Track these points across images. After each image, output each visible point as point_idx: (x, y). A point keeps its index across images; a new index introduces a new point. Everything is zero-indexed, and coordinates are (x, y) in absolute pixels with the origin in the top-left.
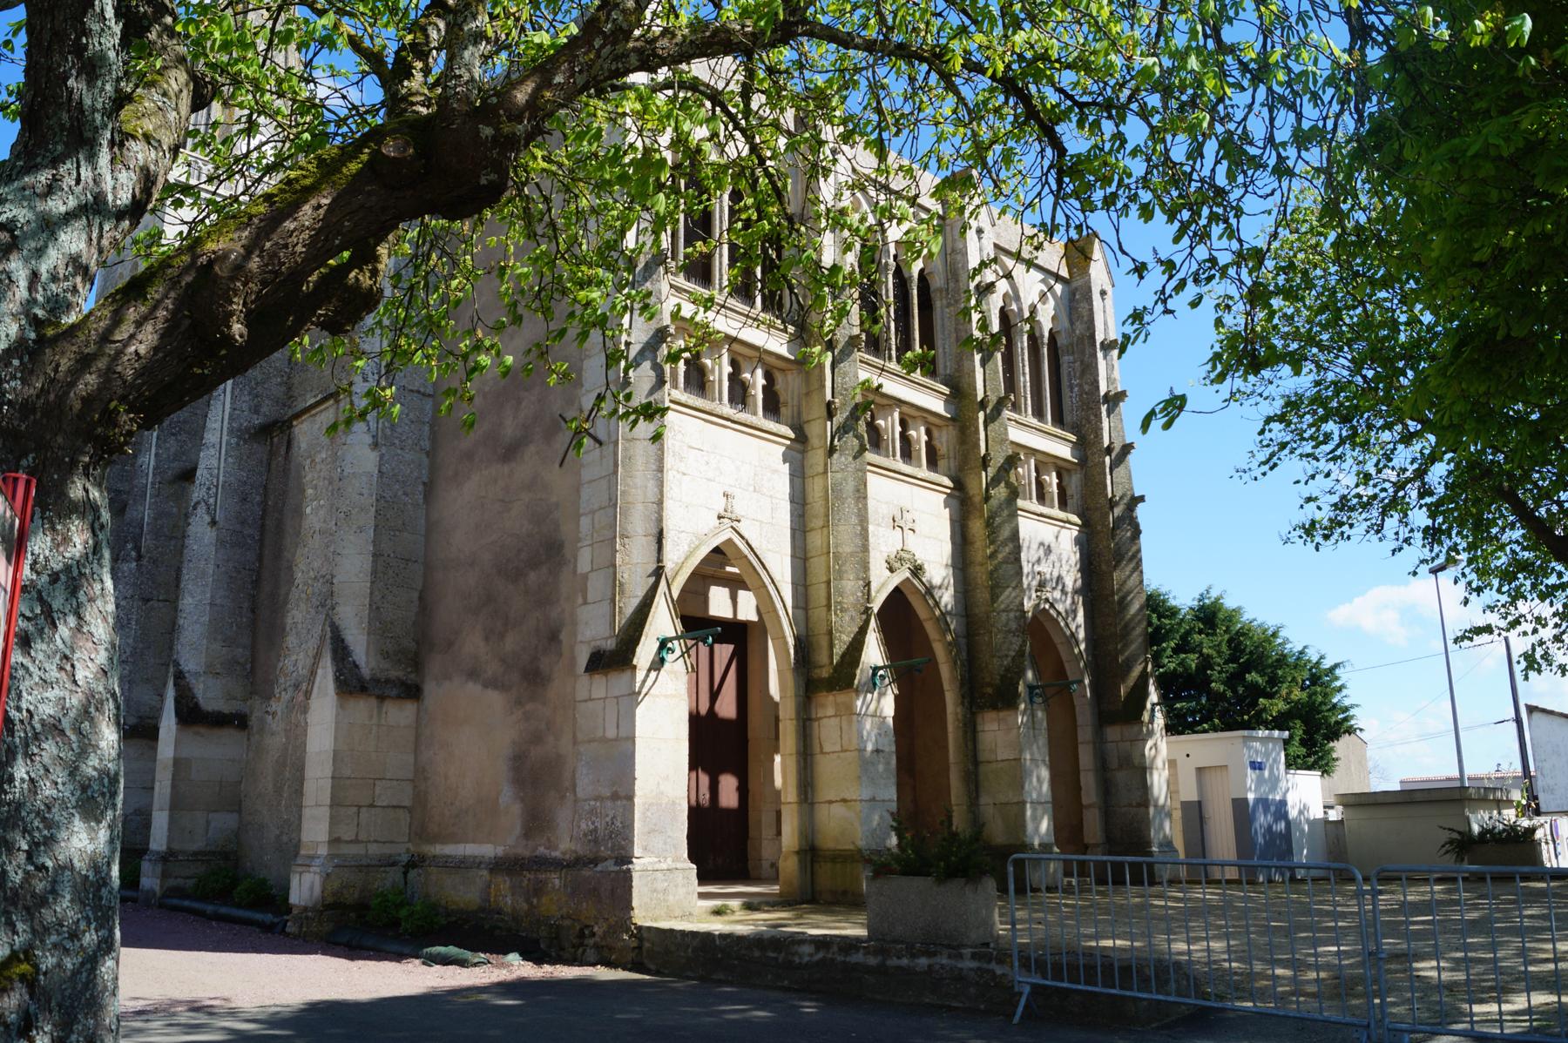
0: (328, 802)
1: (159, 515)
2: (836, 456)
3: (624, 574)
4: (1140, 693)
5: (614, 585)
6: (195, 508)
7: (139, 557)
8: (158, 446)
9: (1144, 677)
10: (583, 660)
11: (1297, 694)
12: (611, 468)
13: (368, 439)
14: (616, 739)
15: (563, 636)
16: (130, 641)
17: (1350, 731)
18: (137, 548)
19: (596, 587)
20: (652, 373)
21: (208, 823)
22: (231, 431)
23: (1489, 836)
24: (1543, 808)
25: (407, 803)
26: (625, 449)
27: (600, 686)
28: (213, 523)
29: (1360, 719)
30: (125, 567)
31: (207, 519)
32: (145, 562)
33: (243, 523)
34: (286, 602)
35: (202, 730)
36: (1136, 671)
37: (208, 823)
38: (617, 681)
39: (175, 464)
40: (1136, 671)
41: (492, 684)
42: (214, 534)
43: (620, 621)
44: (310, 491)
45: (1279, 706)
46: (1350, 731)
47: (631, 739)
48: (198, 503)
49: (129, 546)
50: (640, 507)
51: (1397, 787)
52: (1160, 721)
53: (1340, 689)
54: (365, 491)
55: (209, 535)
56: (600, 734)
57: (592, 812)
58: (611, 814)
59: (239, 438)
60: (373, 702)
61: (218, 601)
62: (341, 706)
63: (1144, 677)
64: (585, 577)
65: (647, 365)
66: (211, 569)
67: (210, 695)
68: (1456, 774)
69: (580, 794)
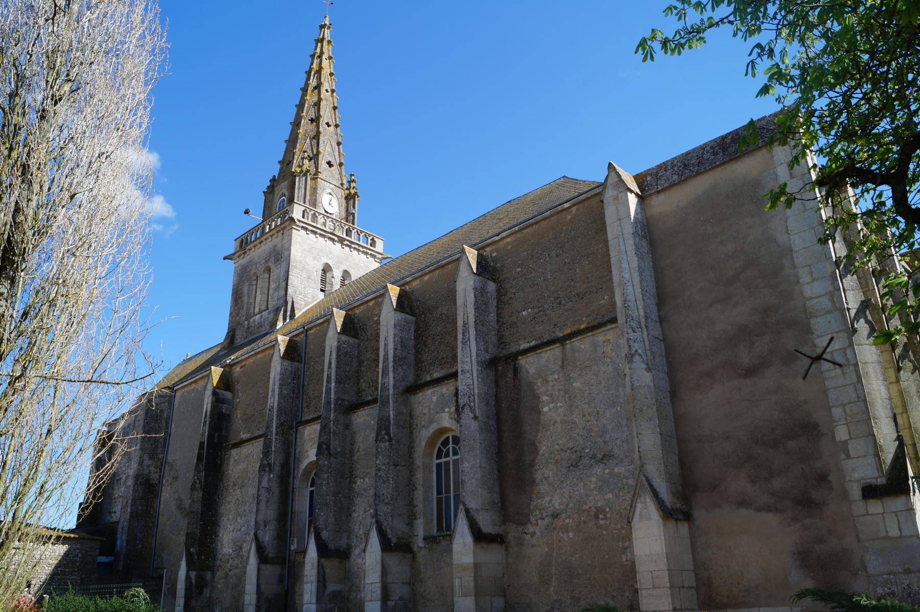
0: (668, 585)
1: (398, 414)
2: (902, 372)
3: (881, 440)
5: (877, 450)
6: (463, 408)
7: (390, 440)
8: (394, 372)
10: (855, 492)
12: (855, 379)
13: (644, 366)
14: (901, 537)
15: (831, 478)
16: (390, 491)
18: (388, 434)
19: (856, 447)
20: (866, 326)
21: (492, 603)
22: (478, 363)
24: (852, 454)
25: (694, 585)
26: (863, 369)
27: (875, 507)
28: (476, 418)
30: (382, 445)
31: (471, 415)
32: (393, 442)
33: (488, 418)
34: (532, 464)
35: (484, 545)
37: (492, 603)
38: (897, 503)
39: (403, 383)
41: (767, 508)
42: (477, 424)
44: (545, 398)
48: (464, 406)
49: (383, 432)
50: (879, 401)
54: (648, 396)
55: (474, 425)
56: (883, 534)
57: (886, 582)
58: (907, 582)
59: (482, 367)
60: (674, 522)
61: (483, 465)
62: (664, 526)
64: (845, 443)
65: (862, 321)
66: (477, 445)
67: (487, 524)
69: (871, 570)
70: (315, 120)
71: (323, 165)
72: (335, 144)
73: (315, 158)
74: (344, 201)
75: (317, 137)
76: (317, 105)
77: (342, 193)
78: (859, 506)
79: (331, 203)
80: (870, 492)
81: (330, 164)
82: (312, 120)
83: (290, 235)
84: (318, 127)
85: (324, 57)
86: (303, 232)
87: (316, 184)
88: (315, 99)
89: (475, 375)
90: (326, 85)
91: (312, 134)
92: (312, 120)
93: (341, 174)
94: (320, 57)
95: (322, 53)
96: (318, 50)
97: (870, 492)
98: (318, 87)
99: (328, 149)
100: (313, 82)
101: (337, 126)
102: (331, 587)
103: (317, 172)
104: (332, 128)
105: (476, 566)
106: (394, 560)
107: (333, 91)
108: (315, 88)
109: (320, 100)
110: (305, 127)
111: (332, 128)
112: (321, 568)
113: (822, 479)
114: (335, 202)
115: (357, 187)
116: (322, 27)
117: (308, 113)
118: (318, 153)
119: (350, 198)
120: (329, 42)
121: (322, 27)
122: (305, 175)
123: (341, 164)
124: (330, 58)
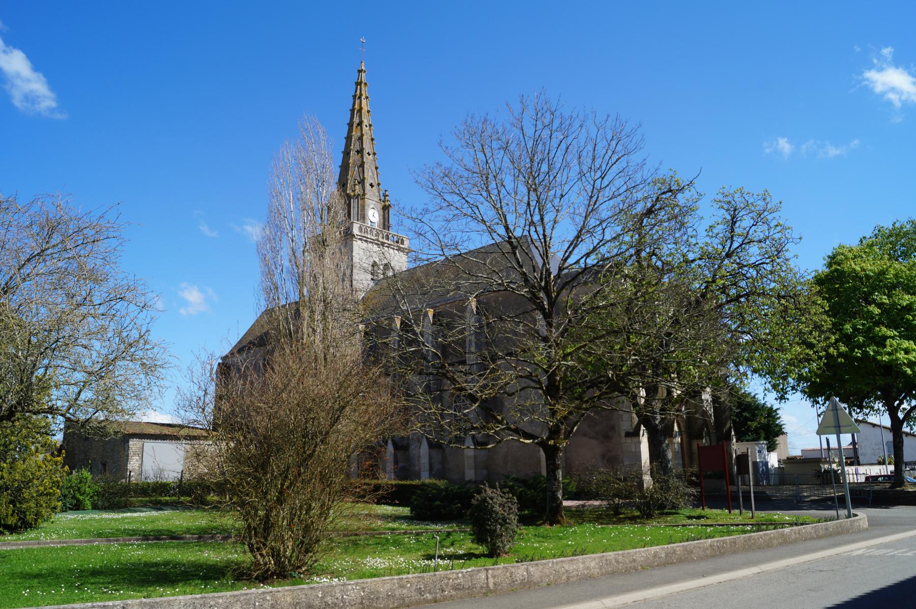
4: (729, 431)
9: (730, 428)
10: (623, 434)
11: (763, 421)
17: (783, 433)
23: (827, 472)
24: (861, 462)
27: (629, 440)
29: (786, 429)
36: (728, 426)
38: (635, 439)
40: (728, 426)
41: (593, 438)
43: (634, 426)
45: (754, 425)
46: (783, 433)
47: (640, 452)
51: (799, 454)
52: (735, 440)
53: (779, 418)
63: (730, 428)
68: (819, 447)
70: (360, 152)
71: (368, 187)
72: (374, 169)
73: (362, 182)
74: (381, 211)
75: (362, 165)
76: (361, 139)
77: (380, 206)
78: (624, 440)
79: (374, 215)
80: (628, 435)
81: (372, 185)
82: (358, 152)
83: (352, 245)
84: (362, 157)
85: (363, 97)
86: (359, 242)
87: (364, 202)
88: (359, 134)
89: (236, 593)
90: (365, 122)
91: (359, 163)
92: (358, 152)
93: (379, 191)
94: (360, 98)
95: (361, 95)
96: (358, 92)
97: (628, 435)
98: (360, 124)
99: (370, 174)
100: (356, 120)
101: (374, 154)
102: (401, 465)
103: (364, 194)
104: (371, 156)
105: (475, 457)
106: (435, 453)
107: (370, 126)
108: (358, 125)
109: (362, 135)
110: (354, 157)
111: (371, 156)
112: (395, 455)
113: (613, 428)
114: (376, 215)
115: (391, 200)
116: (360, 71)
117: (355, 146)
118: (364, 179)
119: (386, 209)
120: (366, 84)
121: (360, 71)
122: (357, 197)
123: (379, 184)
124: (367, 98)
